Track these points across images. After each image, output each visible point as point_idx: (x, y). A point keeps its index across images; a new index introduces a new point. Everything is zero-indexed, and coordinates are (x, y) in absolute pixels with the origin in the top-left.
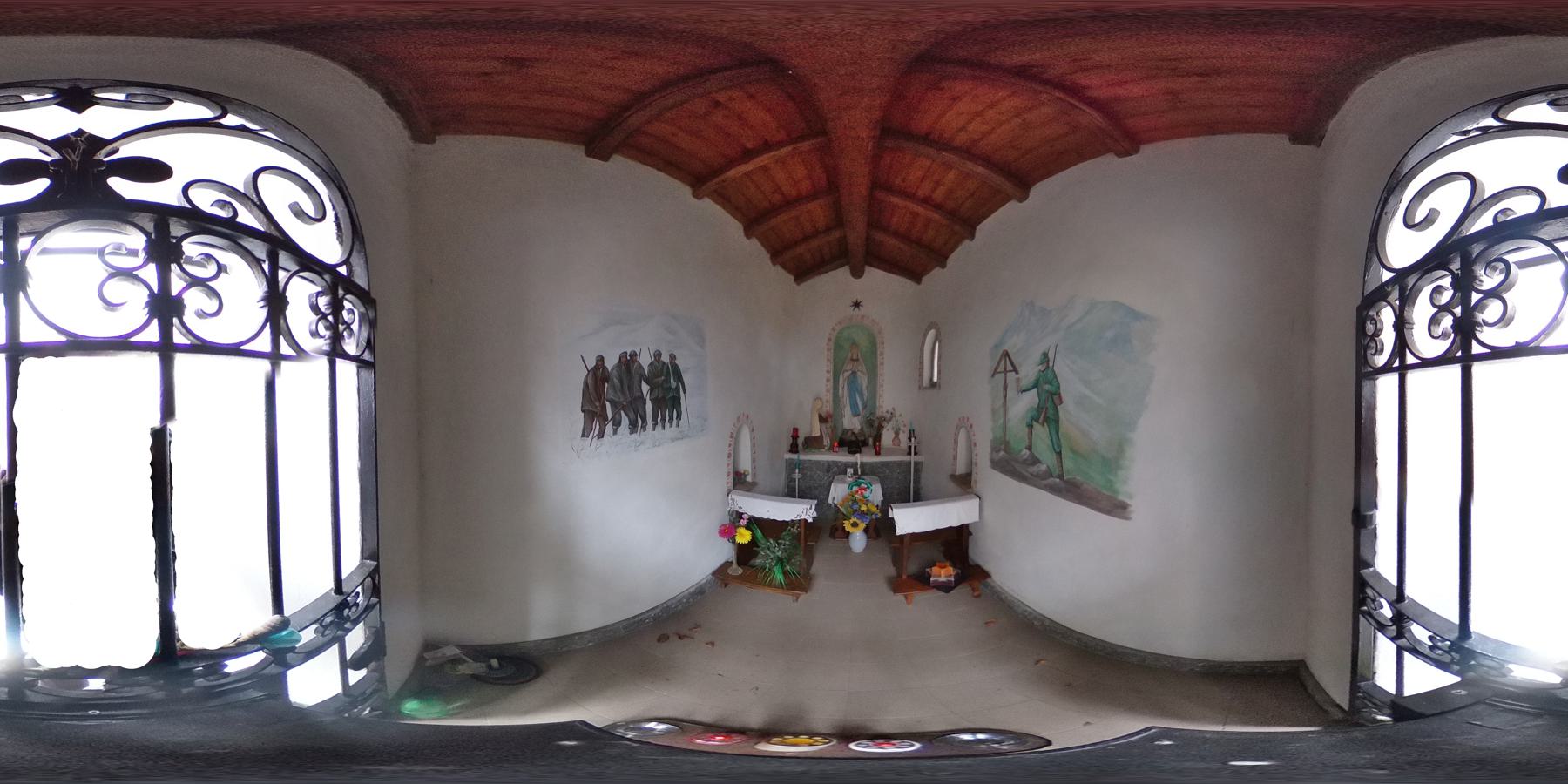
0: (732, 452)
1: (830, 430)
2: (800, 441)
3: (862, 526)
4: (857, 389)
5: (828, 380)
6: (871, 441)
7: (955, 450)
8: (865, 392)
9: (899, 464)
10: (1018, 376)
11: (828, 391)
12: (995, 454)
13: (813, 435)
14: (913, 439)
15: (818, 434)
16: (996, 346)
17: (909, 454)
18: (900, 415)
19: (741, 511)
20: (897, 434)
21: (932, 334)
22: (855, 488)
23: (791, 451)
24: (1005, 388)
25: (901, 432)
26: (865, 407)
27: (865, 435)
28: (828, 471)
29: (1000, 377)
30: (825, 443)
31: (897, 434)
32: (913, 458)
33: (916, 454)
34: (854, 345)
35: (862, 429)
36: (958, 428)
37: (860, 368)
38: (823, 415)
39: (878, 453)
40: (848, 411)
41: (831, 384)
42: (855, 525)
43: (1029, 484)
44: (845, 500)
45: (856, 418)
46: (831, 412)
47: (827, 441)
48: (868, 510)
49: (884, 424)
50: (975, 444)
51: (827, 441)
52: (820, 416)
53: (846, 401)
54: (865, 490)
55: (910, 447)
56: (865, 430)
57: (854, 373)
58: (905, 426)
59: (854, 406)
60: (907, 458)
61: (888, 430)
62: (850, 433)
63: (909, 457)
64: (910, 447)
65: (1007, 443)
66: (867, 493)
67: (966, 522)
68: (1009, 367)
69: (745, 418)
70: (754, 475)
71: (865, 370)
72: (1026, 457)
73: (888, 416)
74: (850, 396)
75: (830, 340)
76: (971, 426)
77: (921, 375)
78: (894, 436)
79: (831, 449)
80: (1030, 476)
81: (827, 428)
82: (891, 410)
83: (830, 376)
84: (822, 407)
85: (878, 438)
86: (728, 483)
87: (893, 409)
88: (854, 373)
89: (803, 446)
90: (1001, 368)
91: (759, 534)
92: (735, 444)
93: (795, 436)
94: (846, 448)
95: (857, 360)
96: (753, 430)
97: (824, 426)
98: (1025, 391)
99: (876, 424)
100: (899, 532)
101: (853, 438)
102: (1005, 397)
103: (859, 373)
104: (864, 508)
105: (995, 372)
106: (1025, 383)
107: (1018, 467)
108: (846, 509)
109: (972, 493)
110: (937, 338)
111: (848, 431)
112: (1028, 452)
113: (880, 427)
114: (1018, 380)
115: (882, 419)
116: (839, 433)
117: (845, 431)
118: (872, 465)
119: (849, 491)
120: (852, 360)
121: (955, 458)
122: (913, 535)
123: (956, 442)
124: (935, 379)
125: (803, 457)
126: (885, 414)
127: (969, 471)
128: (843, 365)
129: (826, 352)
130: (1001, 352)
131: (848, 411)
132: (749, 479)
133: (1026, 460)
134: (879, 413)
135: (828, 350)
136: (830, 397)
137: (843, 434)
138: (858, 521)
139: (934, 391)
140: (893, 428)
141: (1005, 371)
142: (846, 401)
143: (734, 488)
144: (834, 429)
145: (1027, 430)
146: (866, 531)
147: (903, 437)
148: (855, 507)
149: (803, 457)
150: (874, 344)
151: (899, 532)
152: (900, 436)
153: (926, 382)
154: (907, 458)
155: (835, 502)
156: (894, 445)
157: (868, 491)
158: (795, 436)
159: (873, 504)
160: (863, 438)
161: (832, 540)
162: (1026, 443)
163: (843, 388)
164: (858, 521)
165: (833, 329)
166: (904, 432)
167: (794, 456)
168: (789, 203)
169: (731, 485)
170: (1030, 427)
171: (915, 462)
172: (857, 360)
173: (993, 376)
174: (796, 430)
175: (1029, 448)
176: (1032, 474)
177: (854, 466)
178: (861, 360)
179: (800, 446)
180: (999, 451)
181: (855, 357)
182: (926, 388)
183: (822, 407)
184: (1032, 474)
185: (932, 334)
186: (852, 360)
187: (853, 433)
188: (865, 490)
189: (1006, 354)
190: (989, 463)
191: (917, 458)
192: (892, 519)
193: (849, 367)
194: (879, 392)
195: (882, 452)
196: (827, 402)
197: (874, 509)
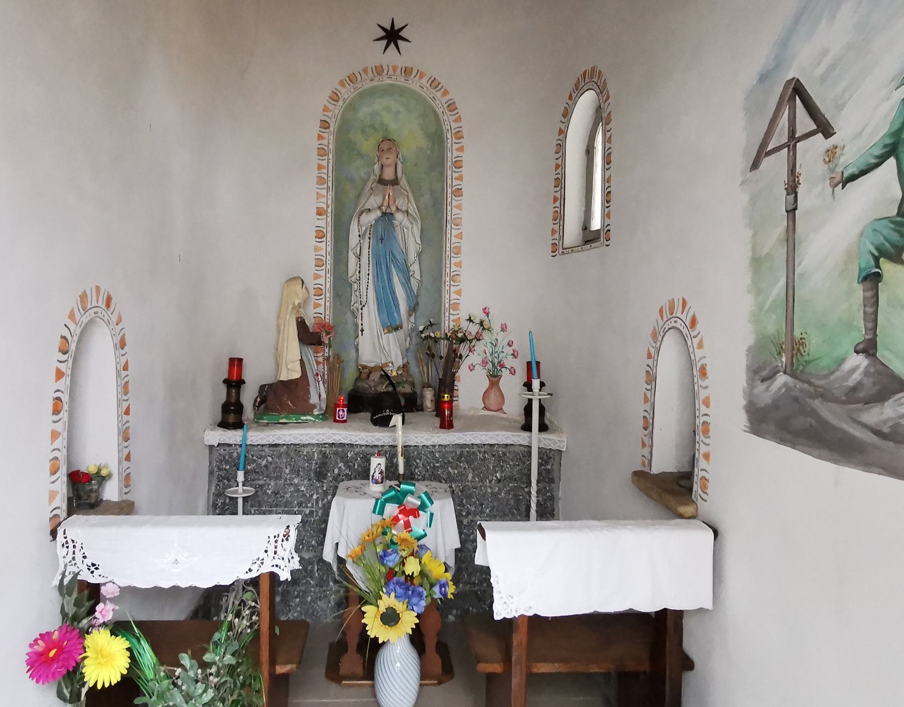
0: (65, 398)
1: (324, 369)
2: (248, 397)
3: (409, 620)
4: (394, 260)
5: (320, 235)
6: (429, 396)
7: (649, 400)
8: (415, 268)
9: (499, 453)
10: (832, 140)
11: (319, 263)
12: (760, 387)
13: (284, 377)
14: (536, 384)
15: (297, 375)
16: (764, 78)
17: (527, 427)
18: (504, 328)
19: (92, 580)
20: (494, 378)
21: (587, 101)
22: (391, 509)
23: (224, 424)
24: (792, 188)
25: (505, 373)
26: (413, 309)
27: (413, 384)
28: (320, 475)
29: (777, 165)
30: (314, 399)
31: (494, 378)
32: (536, 440)
33: (543, 428)
34: (388, 144)
35: (405, 367)
36: (657, 336)
37: (401, 202)
38: (310, 322)
39: (447, 424)
40: (370, 318)
41: (326, 247)
42: (390, 618)
43: (868, 465)
44: (367, 543)
45: (393, 335)
46: (329, 319)
47: (318, 394)
48: (422, 574)
49: (463, 349)
50: (703, 373)
51: (318, 394)
52: (301, 324)
53: (367, 291)
54: (416, 516)
55: (528, 410)
56: (414, 369)
57: (387, 216)
58: (515, 355)
59: (386, 303)
60: (519, 438)
61: (472, 368)
62: (375, 376)
63: (525, 434)
64: (528, 410)
65: (796, 347)
66: (419, 525)
67: (673, 606)
68: (805, 123)
69: (102, 303)
70: (127, 480)
71: (413, 209)
72: (857, 376)
73: (473, 329)
74: (378, 276)
75: (325, 125)
76: (694, 322)
77: (559, 217)
78: (486, 383)
79: (329, 415)
80: (874, 439)
81: (316, 360)
82: (479, 315)
83: (326, 223)
84: (306, 301)
85: (447, 384)
86: (52, 495)
87: (486, 312)
88: (387, 216)
89: (257, 406)
90: (780, 136)
91: (148, 656)
92: (74, 368)
93: (234, 383)
94: (368, 415)
95: (395, 182)
96: (123, 344)
97: (309, 351)
98: (853, 178)
99: (443, 348)
100: (501, 611)
101: (383, 388)
102: (792, 212)
103: (399, 216)
104: (412, 567)
105: (762, 152)
106: (849, 160)
107: (828, 412)
108: (368, 569)
109: (693, 517)
110: (600, 117)
111: (371, 370)
112: (861, 361)
113: (453, 360)
114: (831, 154)
115: (459, 339)
116: (349, 382)
117: (364, 372)
118: (430, 450)
119: (377, 518)
120: (382, 181)
121: (648, 425)
122: (536, 622)
123: (651, 378)
124: (596, 224)
125: (258, 436)
126: (464, 325)
127: (687, 469)
128: (359, 196)
129: (315, 160)
130: (779, 89)
131: (370, 318)
132: (111, 492)
133: (855, 389)
134: (448, 324)
135: (322, 152)
136: (326, 281)
137: (358, 379)
138: (400, 606)
139: (592, 253)
140: (485, 363)
141: (793, 139)
142: (367, 291)
143: (70, 513)
144: (335, 365)
145: (859, 292)
146: (417, 639)
147: (512, 385)
148: (392, 561)
149: (258, 436)
150: (437, 139)
151: (501, 611)
152: (502, 384)
153: (572, 232)
154: (519, 438)
155: (342, 553)
156: (486, 408)
157: (424, 516)
158: (234, 383)
159: (435, 557)
160: (407, 389)
161: (333, 686)
162: (859, 335)
163: (359, 257)
164: (400, 606)
165: (335, 97)
166: (513, 372)
167: (233, 437)
168: (288, 326)
169: (61, 502)
170: (872, 279)
171: (541, 451)
172: (395, 182)
173: (755, 165)
174: (236, 363)
175: (868, 348)
176: (877, 433)
177: (389, 453)
178: (403, 182)
179: (249, 412)
180: (771, 377)
181: (389, 174)
182: (572, 249)
183: (306, 301)
184: (877, 433)
185: (587, 101)
186: (382, 181)
187: (386, 376)
188: (416, 516)
189: (797, 90)
190: (742, 419)
191: (550, 440)
192: (486, 571)
193: (374, 201)
194: (450, 267)
195: (455, 423)
196: (319, 292)
197: (437, 571)
